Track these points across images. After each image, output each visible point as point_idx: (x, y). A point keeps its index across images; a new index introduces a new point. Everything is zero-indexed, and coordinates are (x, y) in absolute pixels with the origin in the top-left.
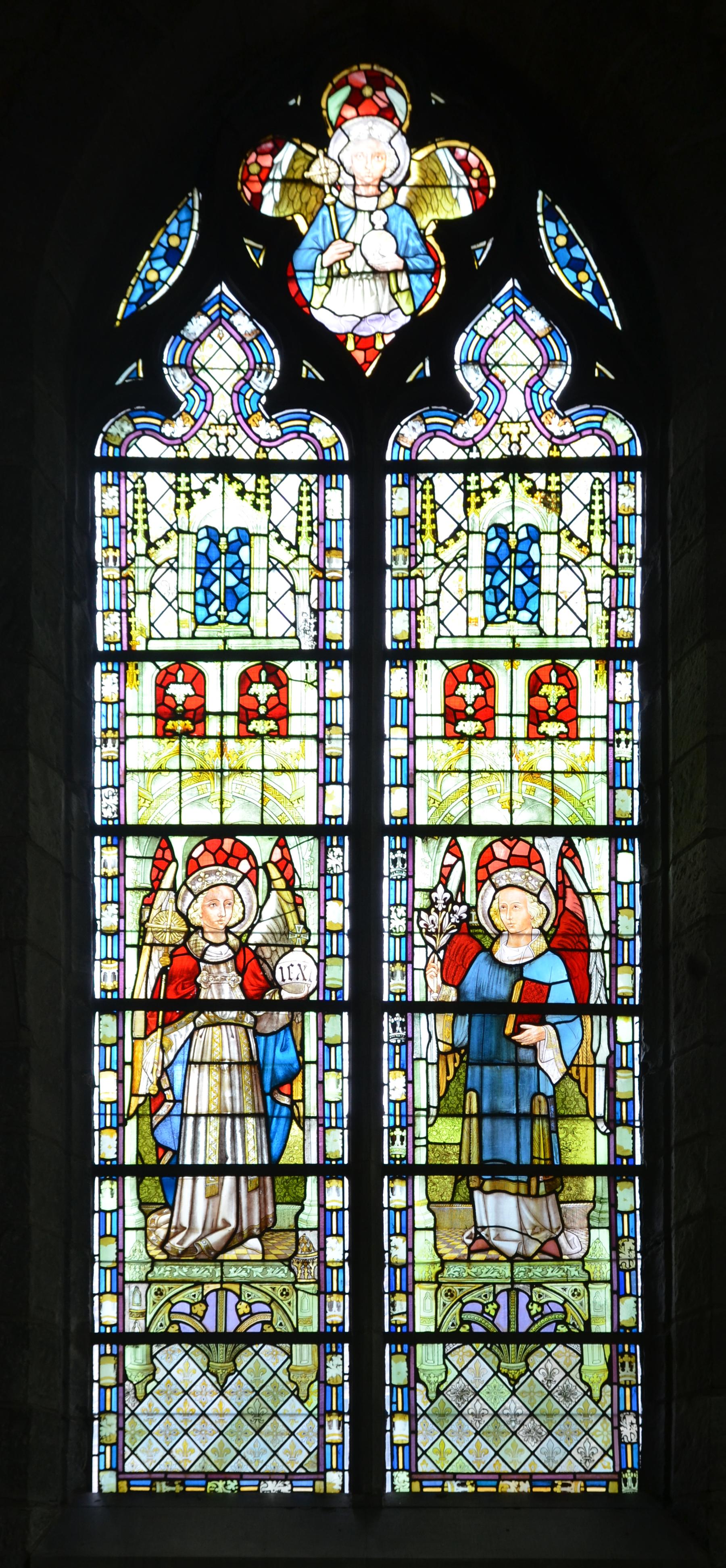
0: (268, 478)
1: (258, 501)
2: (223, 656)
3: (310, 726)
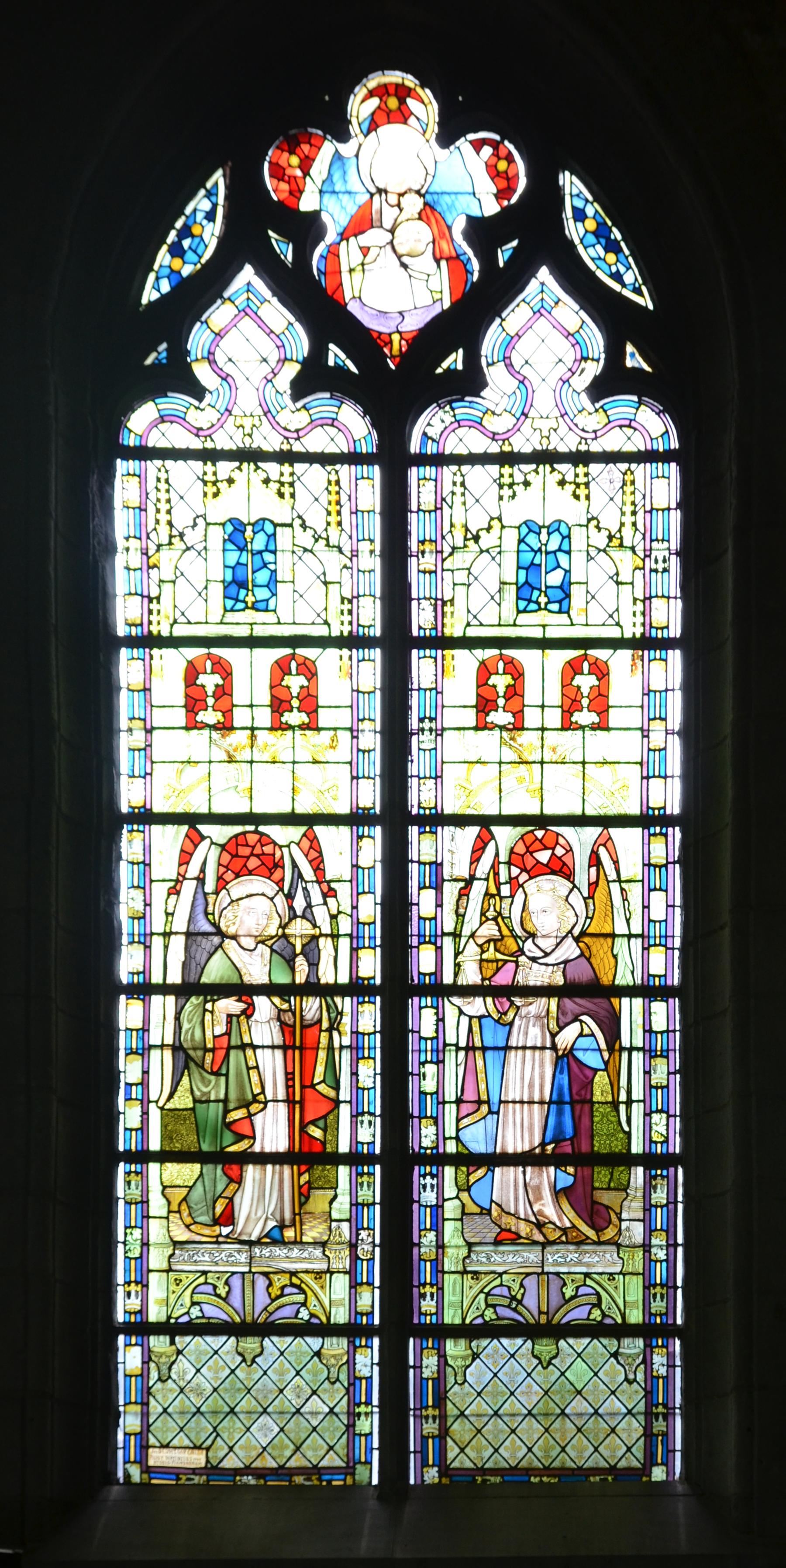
0: (214, 464)
1: (578, 492)
2: (252, 642)
3: (635, 718)
